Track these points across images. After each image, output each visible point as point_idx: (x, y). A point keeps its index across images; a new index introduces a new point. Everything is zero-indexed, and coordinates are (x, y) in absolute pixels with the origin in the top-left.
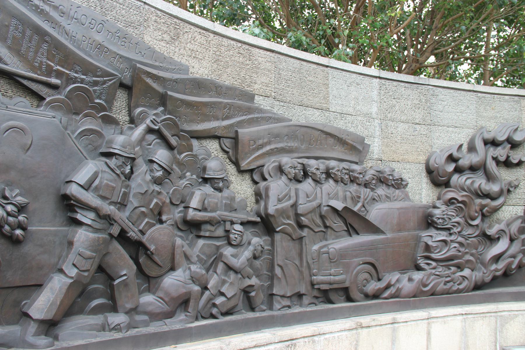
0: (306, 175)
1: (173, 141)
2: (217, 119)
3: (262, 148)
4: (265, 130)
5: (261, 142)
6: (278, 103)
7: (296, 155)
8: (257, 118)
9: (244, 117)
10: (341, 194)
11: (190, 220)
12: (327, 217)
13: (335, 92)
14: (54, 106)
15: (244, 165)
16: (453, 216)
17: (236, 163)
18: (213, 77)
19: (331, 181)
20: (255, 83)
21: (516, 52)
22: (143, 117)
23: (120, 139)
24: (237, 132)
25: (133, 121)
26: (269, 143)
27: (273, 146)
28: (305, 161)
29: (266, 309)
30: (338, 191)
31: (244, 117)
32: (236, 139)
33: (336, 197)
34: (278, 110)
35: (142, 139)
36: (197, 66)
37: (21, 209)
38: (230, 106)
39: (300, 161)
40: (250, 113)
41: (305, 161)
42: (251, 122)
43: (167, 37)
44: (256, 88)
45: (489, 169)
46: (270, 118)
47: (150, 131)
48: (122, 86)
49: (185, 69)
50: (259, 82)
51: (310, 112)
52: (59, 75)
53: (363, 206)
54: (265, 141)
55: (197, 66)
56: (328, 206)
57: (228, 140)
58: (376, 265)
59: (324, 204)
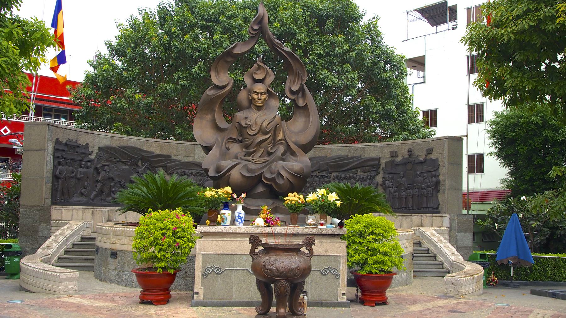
0: (185, 174)
1: (151, 169)
11: (207, 114)
13: (197, 152)
14: (128, 165)
15: (168, 172)
16: (268, 145)
17: (166, 172)
18: (161, 153)
22: (144, 164)
23: (140, 170)
25: (143, 166)
26: (175, 167)
28: (185, 171)
34: (179, 158)
35: (144, 169)
37: (124, 182)
41: (185, 171)
42: (171, 163)
43: (149, 146)
47: (146, 167)
48: (140, 159)
49: (153, 153)
51: (189, 158)
52: (129, 160)
53: (203, 182)
58: (250, 136)
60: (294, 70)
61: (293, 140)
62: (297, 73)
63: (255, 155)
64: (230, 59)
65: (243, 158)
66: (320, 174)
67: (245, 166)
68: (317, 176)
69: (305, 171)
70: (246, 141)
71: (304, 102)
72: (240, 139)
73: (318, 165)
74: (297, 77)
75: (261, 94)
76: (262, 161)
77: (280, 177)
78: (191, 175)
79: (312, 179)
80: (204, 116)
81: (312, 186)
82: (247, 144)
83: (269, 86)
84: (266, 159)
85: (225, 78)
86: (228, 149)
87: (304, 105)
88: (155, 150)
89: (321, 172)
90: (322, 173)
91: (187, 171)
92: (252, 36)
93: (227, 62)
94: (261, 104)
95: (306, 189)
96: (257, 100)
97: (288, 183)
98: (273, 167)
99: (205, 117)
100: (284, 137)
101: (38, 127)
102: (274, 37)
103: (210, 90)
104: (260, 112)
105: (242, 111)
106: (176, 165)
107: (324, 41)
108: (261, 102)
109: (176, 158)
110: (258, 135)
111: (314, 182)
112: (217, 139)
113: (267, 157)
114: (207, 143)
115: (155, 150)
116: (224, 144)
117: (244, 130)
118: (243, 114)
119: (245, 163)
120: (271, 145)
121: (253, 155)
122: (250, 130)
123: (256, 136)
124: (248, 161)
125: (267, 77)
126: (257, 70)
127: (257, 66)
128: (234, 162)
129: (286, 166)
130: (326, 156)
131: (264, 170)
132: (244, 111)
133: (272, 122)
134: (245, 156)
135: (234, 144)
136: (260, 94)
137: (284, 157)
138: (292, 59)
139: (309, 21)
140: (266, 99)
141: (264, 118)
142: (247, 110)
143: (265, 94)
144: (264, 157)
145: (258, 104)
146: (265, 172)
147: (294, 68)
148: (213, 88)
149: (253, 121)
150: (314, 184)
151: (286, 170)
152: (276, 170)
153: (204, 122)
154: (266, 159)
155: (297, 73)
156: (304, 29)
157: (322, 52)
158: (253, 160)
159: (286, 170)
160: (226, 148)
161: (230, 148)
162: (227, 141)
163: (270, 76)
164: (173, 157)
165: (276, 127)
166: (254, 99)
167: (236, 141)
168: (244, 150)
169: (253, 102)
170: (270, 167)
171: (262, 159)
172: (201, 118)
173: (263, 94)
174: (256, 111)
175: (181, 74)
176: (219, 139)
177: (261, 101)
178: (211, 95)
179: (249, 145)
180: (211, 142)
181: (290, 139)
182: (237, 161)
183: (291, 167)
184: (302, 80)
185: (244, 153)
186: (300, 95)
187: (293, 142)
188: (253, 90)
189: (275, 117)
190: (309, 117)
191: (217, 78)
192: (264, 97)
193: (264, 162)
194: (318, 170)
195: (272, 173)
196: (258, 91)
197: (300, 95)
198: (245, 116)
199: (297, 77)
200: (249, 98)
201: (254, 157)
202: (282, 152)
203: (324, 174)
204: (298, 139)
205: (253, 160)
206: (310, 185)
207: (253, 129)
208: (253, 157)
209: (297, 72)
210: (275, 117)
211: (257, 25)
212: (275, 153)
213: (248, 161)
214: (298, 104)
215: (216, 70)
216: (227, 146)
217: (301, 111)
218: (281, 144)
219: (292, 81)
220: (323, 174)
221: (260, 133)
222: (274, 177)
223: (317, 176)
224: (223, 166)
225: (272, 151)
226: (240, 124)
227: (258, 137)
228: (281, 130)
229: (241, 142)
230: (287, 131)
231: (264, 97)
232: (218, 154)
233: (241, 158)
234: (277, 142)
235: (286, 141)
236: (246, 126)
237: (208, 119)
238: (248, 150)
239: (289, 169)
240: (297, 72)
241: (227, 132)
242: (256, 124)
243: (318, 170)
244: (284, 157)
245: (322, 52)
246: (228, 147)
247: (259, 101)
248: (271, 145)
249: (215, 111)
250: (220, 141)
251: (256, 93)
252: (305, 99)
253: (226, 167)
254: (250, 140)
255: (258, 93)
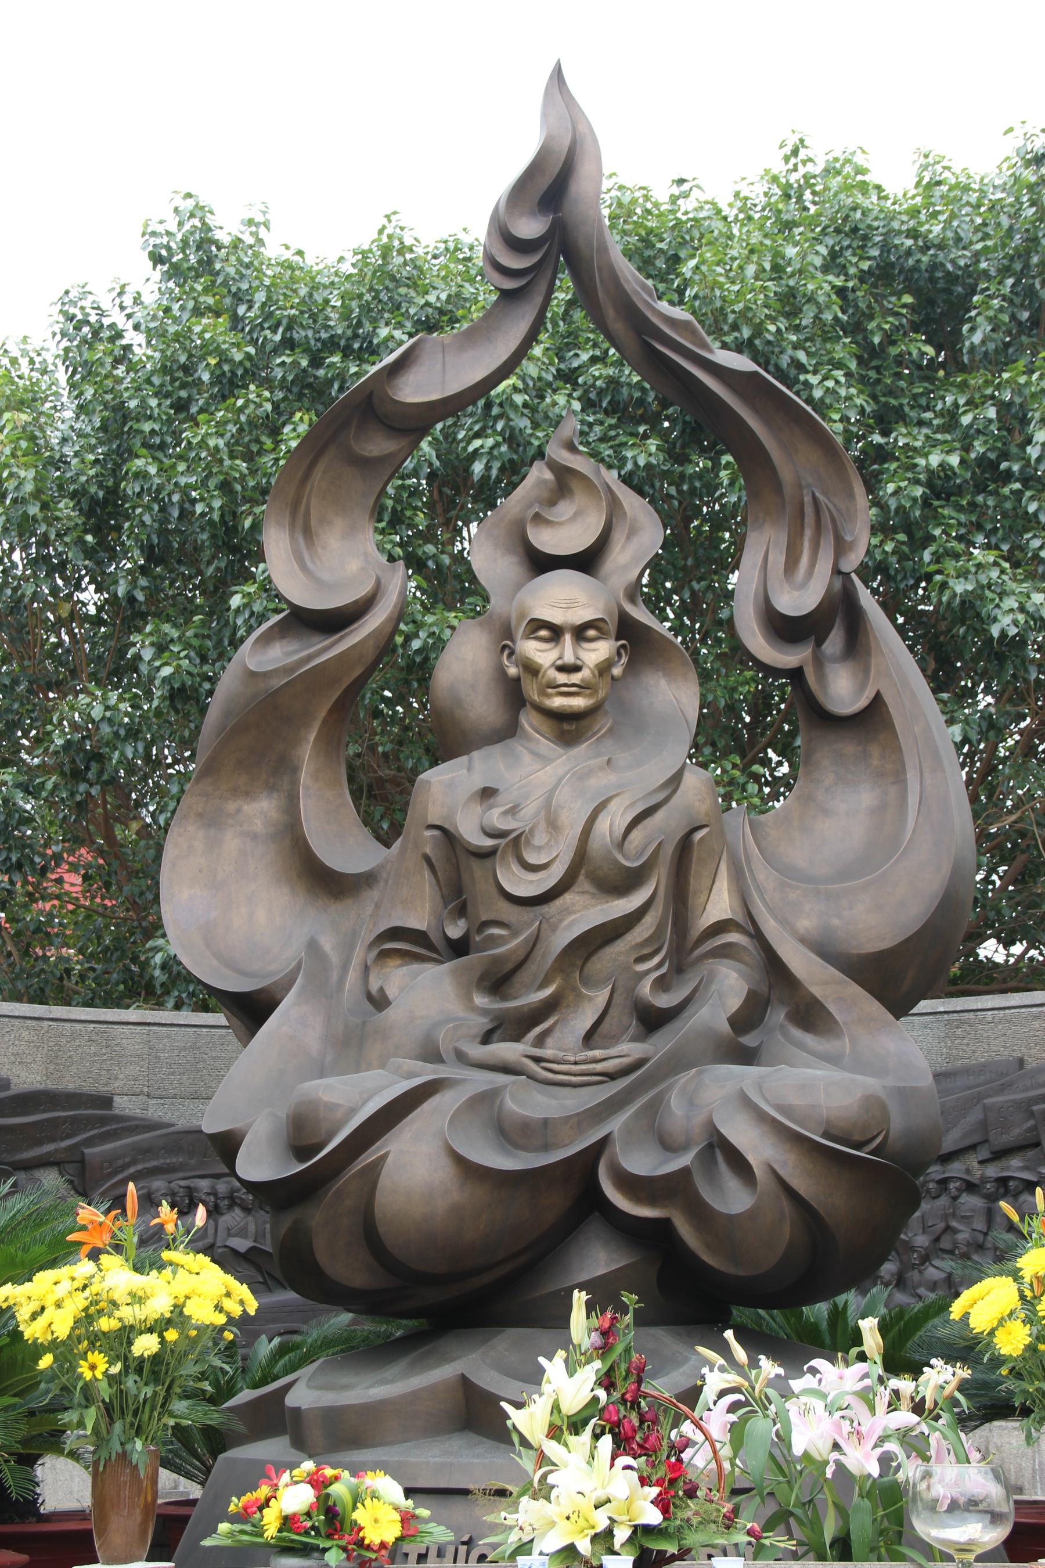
2: (52, 1140)
3: (122, 1171)
4: (127, 1145)
5: (120, 1162)
6: (154, 1101)
7: (181, 1175)
8: (115, 1130)
9: (92, 1133)
10: (252, 1228)
11: (248, 794)
12: (912, 776)
16: (641, 959)
18: (50, 1085)
19: (237, 1211)
20: (116, 1079)
21: (46, 1361)
24: (83, 1153)
26: (134, 1162)
27: (139, 1167)
29: (81, 1414)
30: (247, 1224)
31: (92, 1133)
32: (82, 1161)
33: (242, 1233)
34: (156, 1111)
36: (23, 1074)
38: (73, 1120)
39: (183, 1183)
40: (103, 1126)
42: (105, 1137)
44: (117, 1085)
45: (628, 281)
46: (137, 1126)
50: (121, 1076)
54: (127, 1160)
55: (23, 1074)
56: (226, 1246)
57: (72, 1165)
59: (219, 1244)
60: (788, 490)
61: (805, 924)
62: (809, 510)
63: (557, 1034)
64: (378, 445)
65: (477, 1052)
66: (992, 1171)
67: (486, 1099)
68: (970, 1187)
69: (897, 1123)
70: (494, 941)
71: (862, 687)
72: (455, 931)
73: (975, 1116)
74: (808, 533)
75: (580, 633)
76: (598, 1067)
77: (720, 1158)
78: (230, 1207)
79: (943, 1201)
80: (231, 806)
81: (945, 1243)
82: (497, 960)
83: (633, 592)
84: (628, 1050)
85: (354, 566)
86: (379, 1002)
87: (863, 702)
88: (17, 1070)
89: (1000, 1155)
90: (1003, 1163)
91: (204, 1184)
92: (510, 284)
93: (365, 465)
94: (579, 703)
95: (913, 1267)
96: (553, 673)
97: (786, 1204)
98: (676, 1104)
99: (238, 811)
100: (737, 904)
101: (885, 1429)
102: (644, 287)
103: (266, 639)
104: (581, 750)
105: (463, 759)
106: (145, 1151)
107: (962, 401)
108: (583, 688)
109: (138, 1112)
110: (568, 898)
111: (954, 1224)
112: (313, 947)
113: (635, 1039)
114: (230, 964)
115: (17, 1070)
116: (353, 975)
117: (477, 868)
118: (469, 769)
119: (484, 1080)
120: (656, 960)
121: (538, 1030)
122: (515, 868)
123: (558, 902)
124: (506, 1069)
125: (618, 537)
126: (552, 503)
127: (548, 475)
128: (410, 1075)
129: (760, 1088)
130: (1021, 1062)
131: (615, 1125)
132: (475, 754)
133: (660, 816)
134: (486, 1039)
135: (415, 967)
136: (568, 638)
137: (749, 1040)
138: (767, 422)
139: (863, 305)
140: (617, 671)
141: (603, 781)
142: (497, 749)
143: (603, 635)
144: (613, 1039)
145: (558, 702)
146: (616, 1135)
147: (786, 473)
148: (282, 630)
149: (529, 810)
150: (955, 1231)
151: (762, 1117)
152: (698, 1120)
153: (232, 842)
154: (628, 1050)
155: (809, 510)
156: (843, 349)
157: (954, 460)
158: (537, 1060)
159: (762, 1117)
160: (370, 997)
161: (391, 993)
162: (374, 953)
163: (632, 532)
164: (125, 1105)
165: (685, 845)
166: (532, 669)
167: (429, 945)
168: (481, 1000)
169: (531, 690)
170: (655, 1107)
171: (597, 1053)
172: (213, 821)
173: (591, 633)
174: (546, 745)
175: (175, 634)
176: (328, 944)
177: (576, 678)
178: (266, 675)
179: (509, 966)
180: (273, 967)
181: (784, 922)
182: (428, 1073)
183: (795, 1100)
184: (841, 547)
185: (483, 1023)
186: (834, 642)
187: (803, 941)
188: (522, 615)
189: (675, 780)
190: (899, 776)
191: (303, 567)
192: (596, 652)
193: (612, 1076)
194: (973, 1148)
195: (668, 1146)
196: (556, 617)
197: (834, 642)
198: (478, 781)
199: (808, 533)
200: (502, 672)
201: (550, 1041)
202: (734, 1003)
203: (1015, 1167)
204: (836, 922)
205: (537, 1060)
206: (937, 1239)
207: (532, 859)
208: (540, 1041)
209: (807, 499)
210: (675, 780)
211: (532, 214)
212: (685, 1014)
213: (506, 1069)
214: (821, 698)
215: (300, 522)
216: (374, 987)
217: (849, 748)
218: (726, 952)
219: (778, 559)
220: (1007, 1169)
221: (583, 883)
222: (685, 1172)
223: (970, 1187)
224: (333, 1107)
225: (664, 1001)
226: (449, 837)
227: (567, 911)
228: (723, 867)
229: (459, 948)
230: (763, 874)
231: (596, 652)
232: (312, 1038)
233: (461, 1057)
234: (693, 949)
235: (758, 935)
236: (489, 842)
237: (259, 826)
238: (504, 998)
239: (781, 1109)
240: (807, 499)
241: (374, 894)
242: (553, 825)
243: (973, 1148)
244: (749, 1040)
245: (954, 460)
246: (381, 990)
247: (562, 678)
248: (656, 960)
249: (295, 770)
250: (334, 958)
251: (543, 633)
252: (866, 671)
253: (353, 1111)
254: (515, 934)
255: (556, 632)
